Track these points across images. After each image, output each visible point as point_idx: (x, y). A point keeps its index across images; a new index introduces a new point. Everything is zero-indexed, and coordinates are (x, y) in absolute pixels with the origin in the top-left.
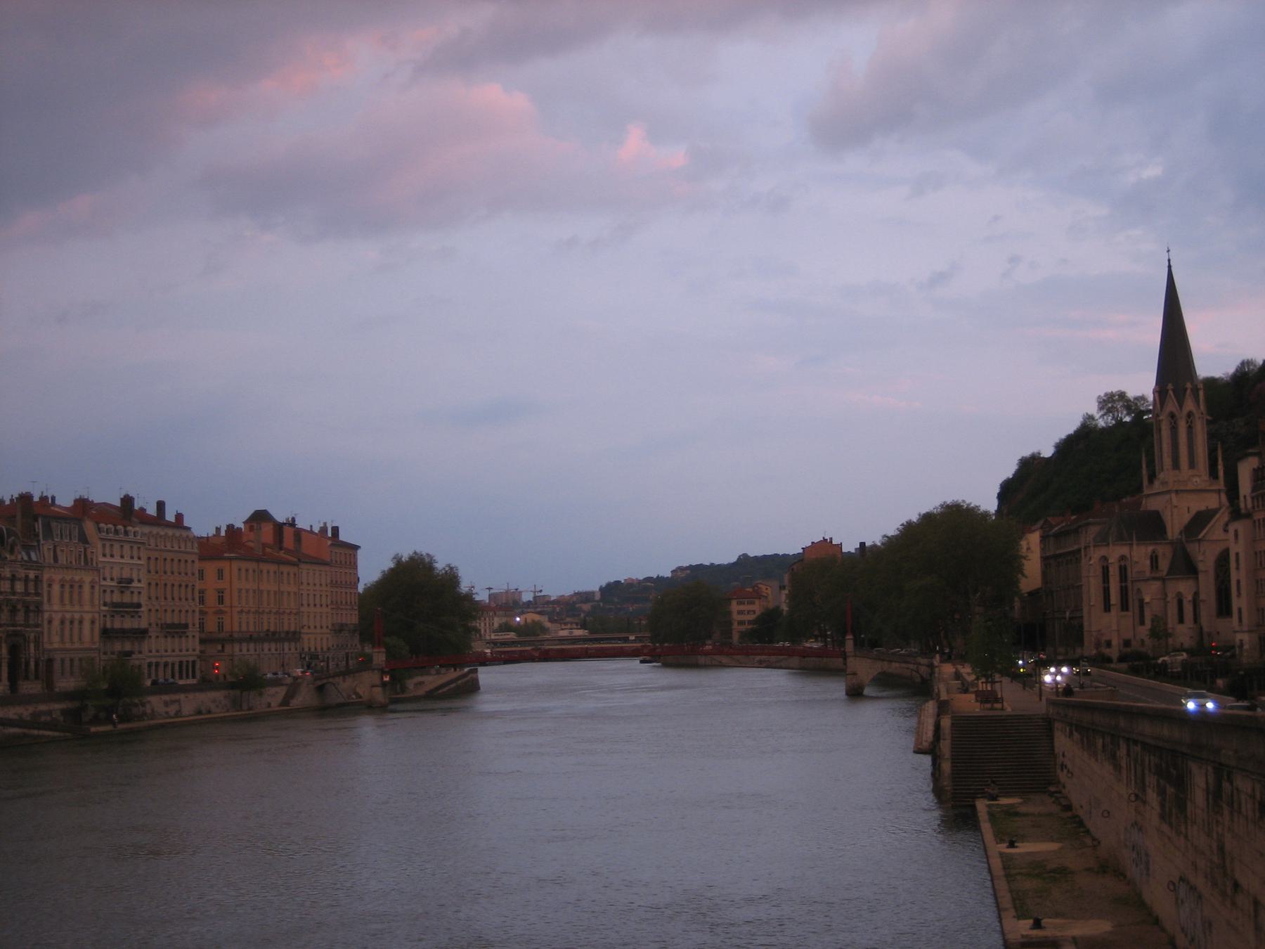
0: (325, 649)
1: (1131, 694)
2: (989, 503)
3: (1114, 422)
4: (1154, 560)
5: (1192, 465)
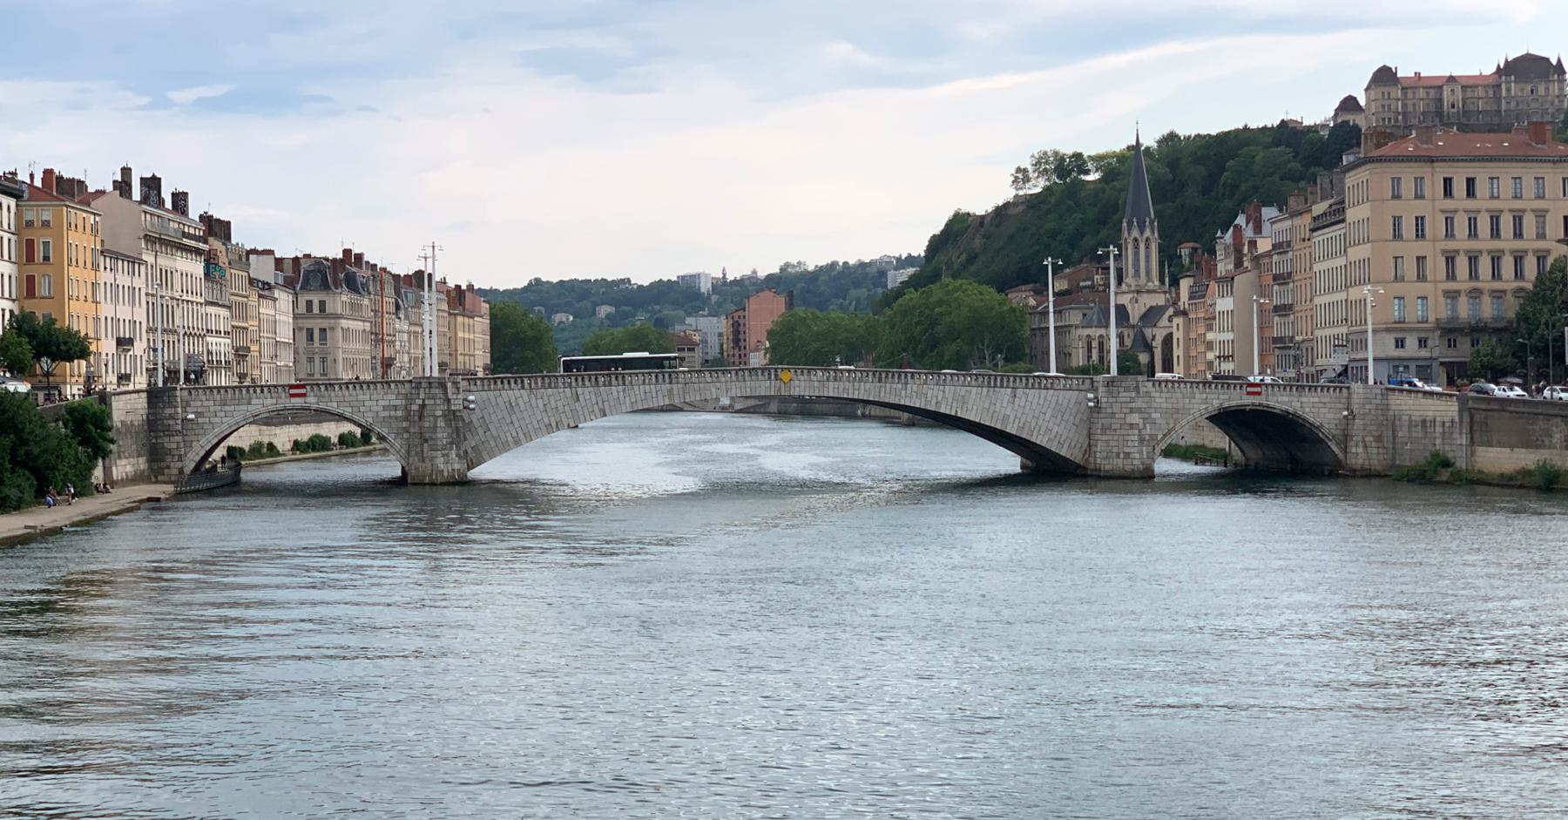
0: (1126, 438)
1: (872, 466)
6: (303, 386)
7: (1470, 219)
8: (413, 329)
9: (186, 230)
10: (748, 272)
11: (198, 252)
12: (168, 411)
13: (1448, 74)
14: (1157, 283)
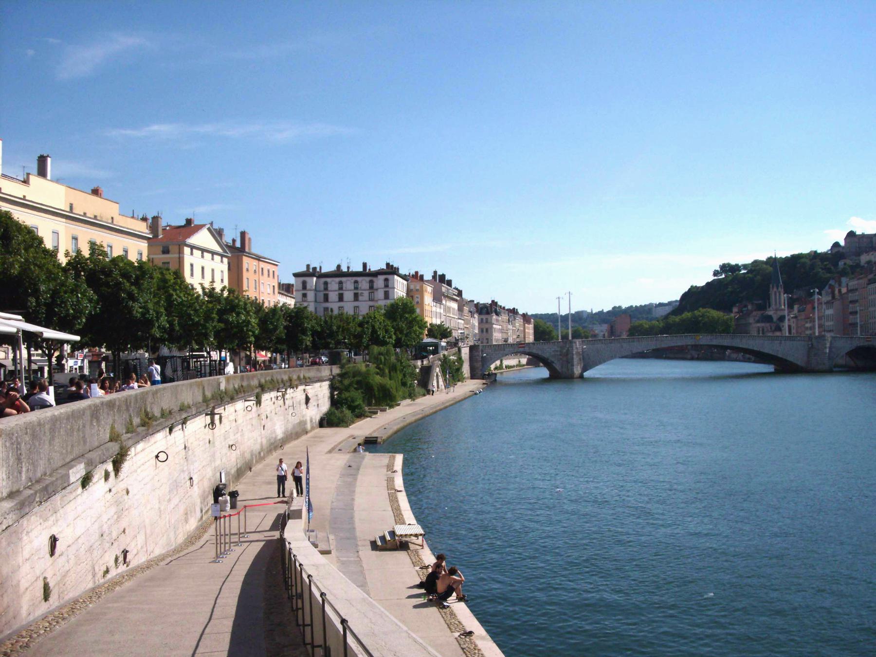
8: (514, 328)
10: (601, 310)
12: (476, 354)
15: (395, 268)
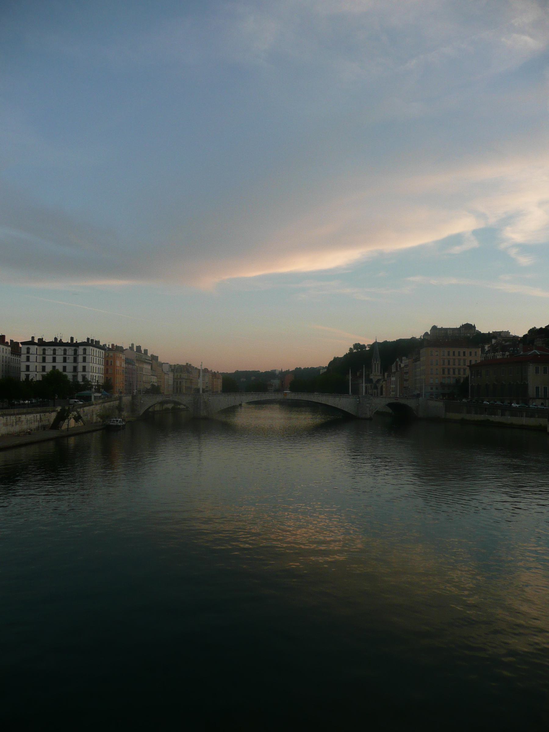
2: (327, 366)
3: (369, 417)
4: (371, 386)
5: (378, 372)
6: (169, 395)
7: (448, 361)
9: (147, 358)
11: (149, 363)
13: (174, 364)
14: (380, 373)
15: (96, 341)
